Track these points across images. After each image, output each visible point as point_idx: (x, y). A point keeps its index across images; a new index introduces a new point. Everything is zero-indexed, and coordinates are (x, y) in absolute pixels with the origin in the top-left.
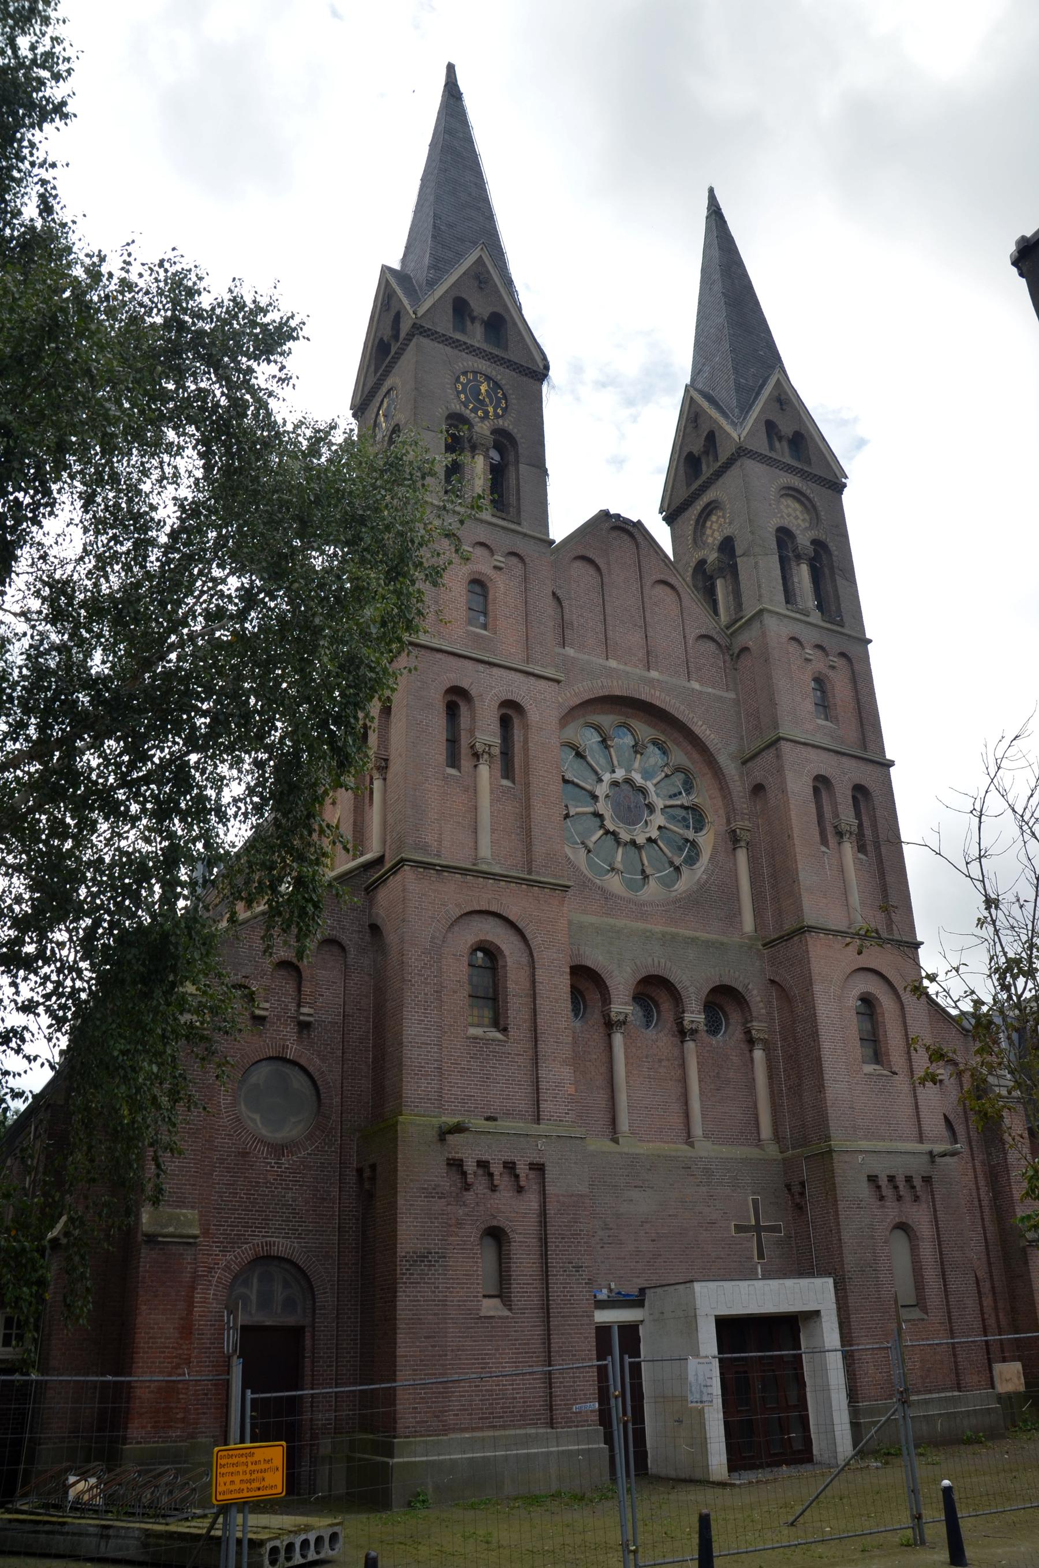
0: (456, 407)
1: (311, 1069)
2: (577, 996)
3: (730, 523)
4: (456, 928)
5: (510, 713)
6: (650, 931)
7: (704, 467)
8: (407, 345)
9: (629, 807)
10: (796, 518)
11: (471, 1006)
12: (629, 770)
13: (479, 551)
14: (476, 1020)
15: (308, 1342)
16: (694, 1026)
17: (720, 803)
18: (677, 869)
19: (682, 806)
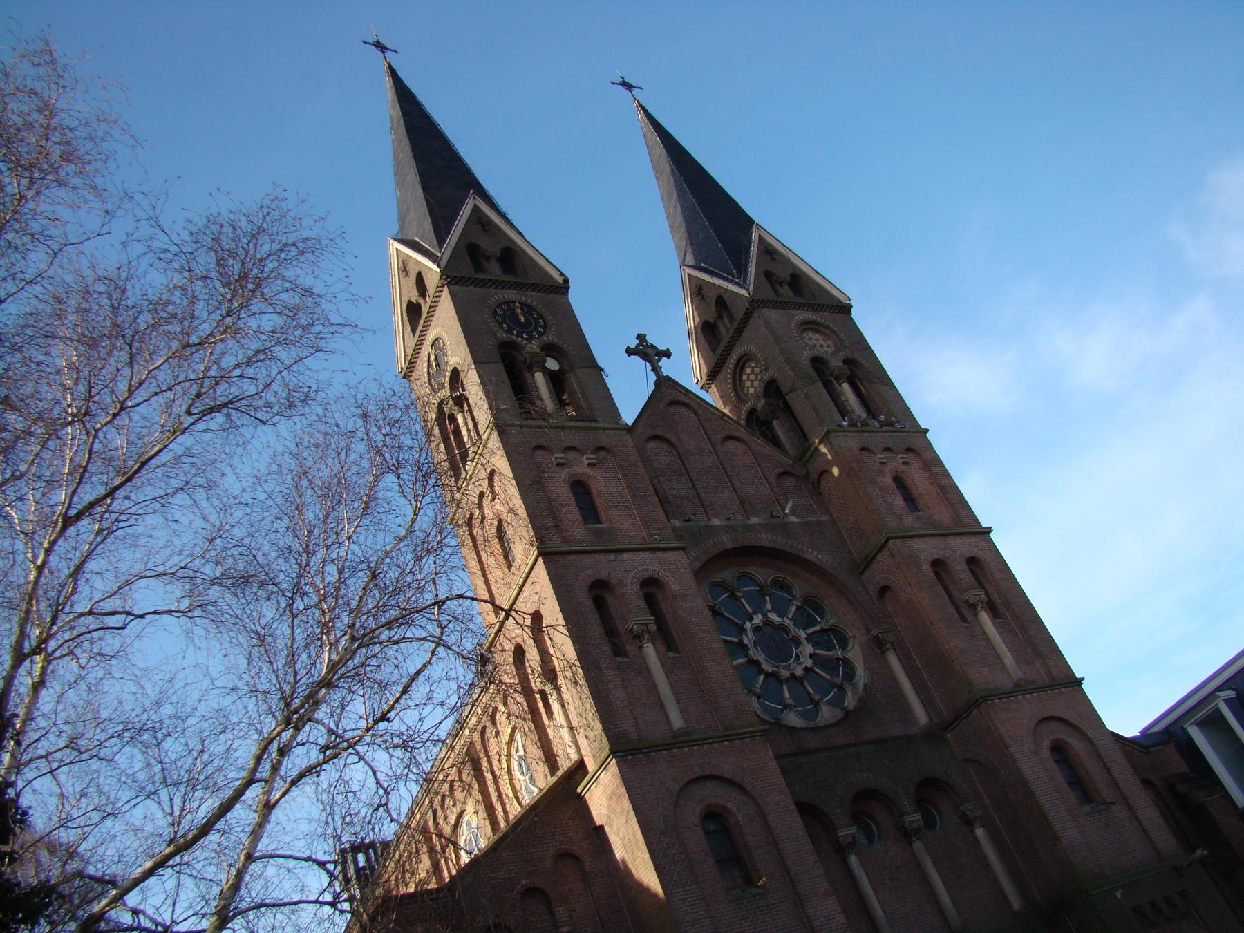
0: (503, 336)
3: (766, 370)
7: (723, 330)
10: (821, 346)
13: (570, 455)
16: (915, 825)
18: (840, 688)
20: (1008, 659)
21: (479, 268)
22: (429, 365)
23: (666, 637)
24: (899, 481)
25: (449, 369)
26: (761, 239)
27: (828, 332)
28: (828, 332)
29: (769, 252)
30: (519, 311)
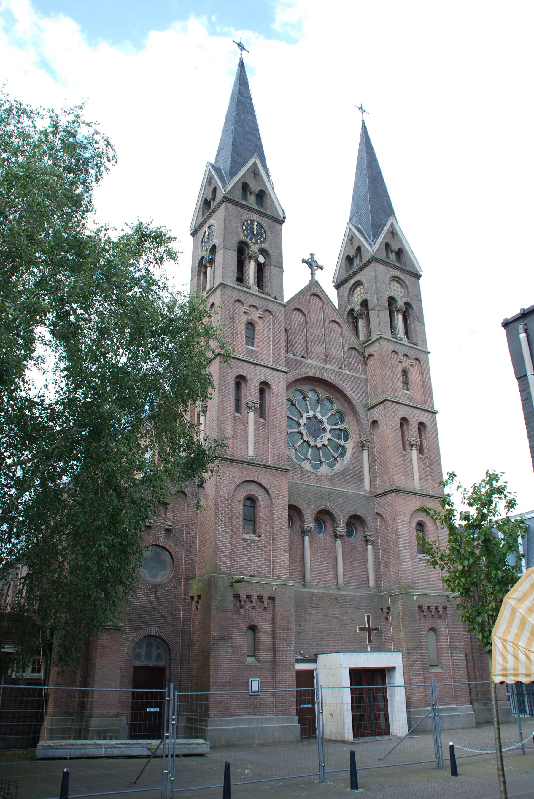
0: (243, 238)
1: (170, 550)
4: (239, 488)
5: (264, 387)
8: (220, 206)
9: (315, 429)
10: (398, 291)
11: (244, 524)
12: (315, 412)
13: (252, 309)
14: (246, 530)
15: (167, 674)
17: (357, 428)
18: (336, 459)
19: (339, 429)
20: (416, 476)
21: (245, 197)
22: (204, 236)
23: (262, 412)
24: (405, 372)
25: (212, 244)
26: (392, 224)
27: (404, 286)
28: (404, 286)
29: (393, 233)
30: (255, 227)
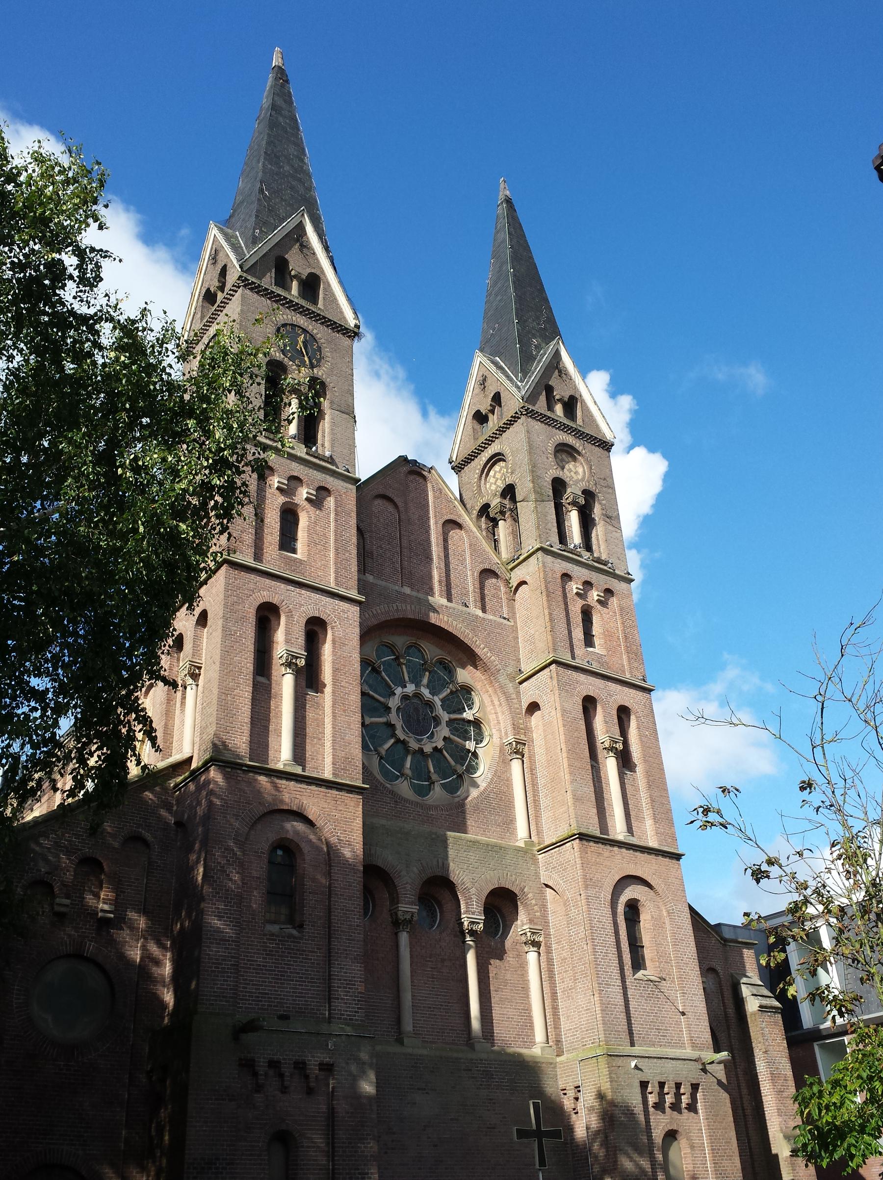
2: (368, 892)
3: (512, 473)
6: (436, 834)
12: (418, 685)
